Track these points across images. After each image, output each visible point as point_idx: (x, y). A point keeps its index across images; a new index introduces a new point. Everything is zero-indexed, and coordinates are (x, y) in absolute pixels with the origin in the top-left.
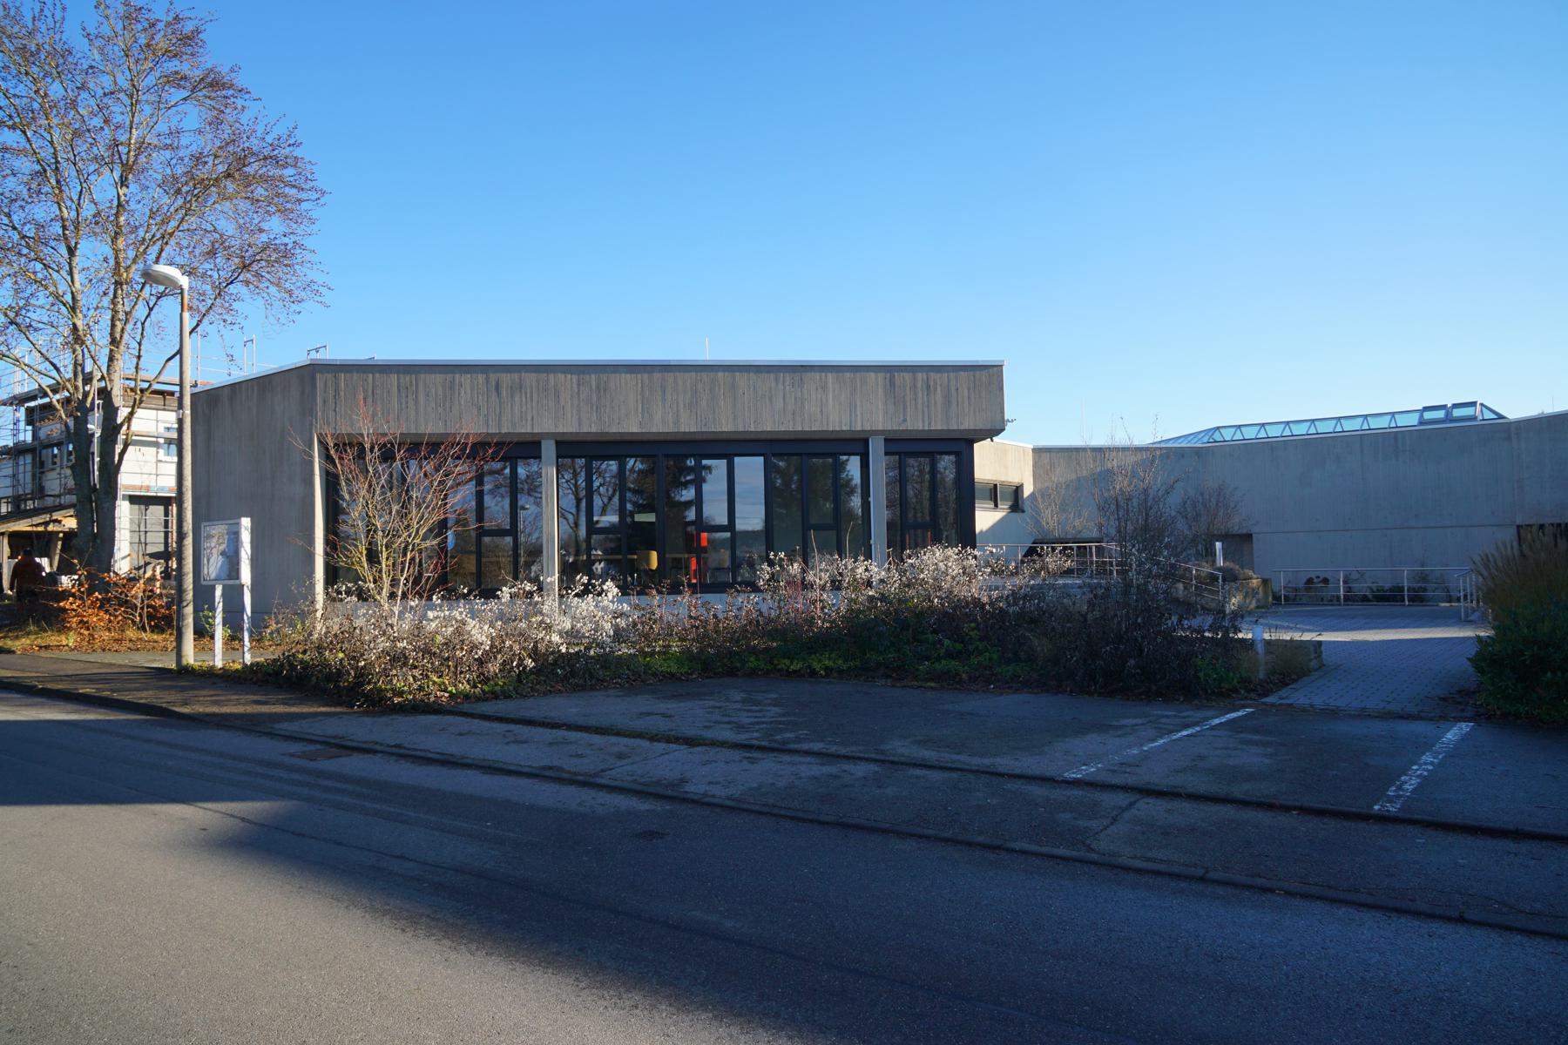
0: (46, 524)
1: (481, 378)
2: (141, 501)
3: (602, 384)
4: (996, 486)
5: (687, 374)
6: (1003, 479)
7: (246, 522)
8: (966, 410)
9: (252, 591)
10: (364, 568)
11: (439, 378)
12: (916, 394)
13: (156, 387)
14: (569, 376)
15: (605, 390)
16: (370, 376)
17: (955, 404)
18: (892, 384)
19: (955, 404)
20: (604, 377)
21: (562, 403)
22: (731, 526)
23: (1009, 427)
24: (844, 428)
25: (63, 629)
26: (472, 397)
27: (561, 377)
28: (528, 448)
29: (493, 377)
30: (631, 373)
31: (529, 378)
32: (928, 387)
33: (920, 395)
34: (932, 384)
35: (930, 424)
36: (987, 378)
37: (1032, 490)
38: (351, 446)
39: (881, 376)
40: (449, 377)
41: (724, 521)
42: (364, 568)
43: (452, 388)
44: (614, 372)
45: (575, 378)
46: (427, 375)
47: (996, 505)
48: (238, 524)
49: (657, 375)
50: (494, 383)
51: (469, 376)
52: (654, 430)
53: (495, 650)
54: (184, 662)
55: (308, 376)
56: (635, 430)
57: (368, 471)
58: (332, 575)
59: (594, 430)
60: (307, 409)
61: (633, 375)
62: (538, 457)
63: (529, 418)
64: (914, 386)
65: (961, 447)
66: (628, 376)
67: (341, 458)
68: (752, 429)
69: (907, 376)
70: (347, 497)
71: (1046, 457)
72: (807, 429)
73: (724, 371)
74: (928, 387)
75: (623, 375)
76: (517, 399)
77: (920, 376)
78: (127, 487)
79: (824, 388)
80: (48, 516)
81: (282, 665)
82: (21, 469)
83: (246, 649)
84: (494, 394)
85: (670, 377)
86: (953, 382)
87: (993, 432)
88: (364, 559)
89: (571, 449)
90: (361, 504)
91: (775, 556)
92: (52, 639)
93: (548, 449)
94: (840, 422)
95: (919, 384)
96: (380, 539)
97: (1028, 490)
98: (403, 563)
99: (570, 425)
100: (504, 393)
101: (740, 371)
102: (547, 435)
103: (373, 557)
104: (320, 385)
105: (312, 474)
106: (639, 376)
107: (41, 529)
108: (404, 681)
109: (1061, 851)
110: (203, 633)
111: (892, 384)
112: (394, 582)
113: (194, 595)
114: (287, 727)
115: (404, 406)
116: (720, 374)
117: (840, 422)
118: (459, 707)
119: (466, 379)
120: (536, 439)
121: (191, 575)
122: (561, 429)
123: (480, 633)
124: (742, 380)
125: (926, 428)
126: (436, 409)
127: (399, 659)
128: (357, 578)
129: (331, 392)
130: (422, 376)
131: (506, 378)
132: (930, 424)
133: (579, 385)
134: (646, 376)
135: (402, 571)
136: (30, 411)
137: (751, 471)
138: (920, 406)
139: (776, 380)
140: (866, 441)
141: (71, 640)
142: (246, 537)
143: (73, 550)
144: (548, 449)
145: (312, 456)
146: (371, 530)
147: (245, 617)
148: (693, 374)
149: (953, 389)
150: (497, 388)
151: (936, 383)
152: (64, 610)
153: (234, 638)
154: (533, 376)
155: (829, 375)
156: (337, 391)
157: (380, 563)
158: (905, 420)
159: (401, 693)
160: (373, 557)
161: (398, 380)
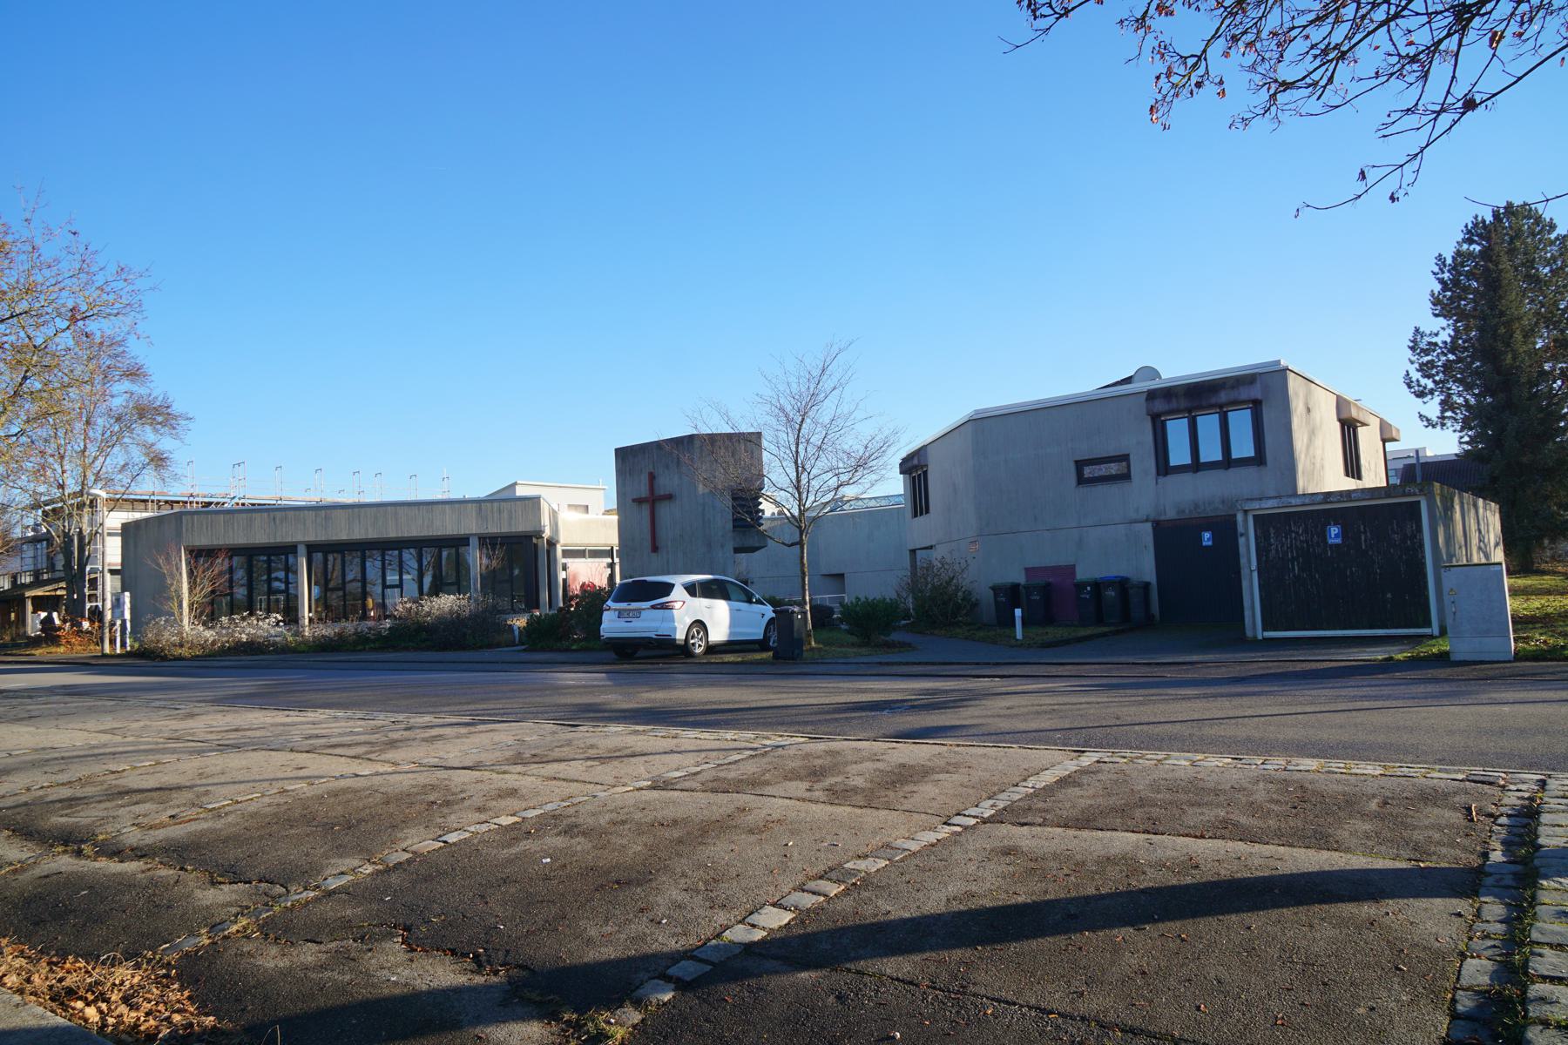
0: (56, 590)
1: (265, 515)
2: (113, 572)
13: (125, 497)
18: (480, 509)
20: (328, 512)
25: (59, 645)
28: (291, 549)
29: (272, 514)
35: (510, 525)
49: (356, 510)
53: (214, 643)
56: (345, 538)
60: (179, 534)
64: (492, 512)
69: (488, 505)
78: (109, 565)
80: (1527, 4)
82: (39, 552)
85: (363, 510)
89: (312, 548)
92: (53, 649)
93: (302, 550)
99: (311, 537)
100: (278, 522)
102: (301, 542)
107: (53, 593)
109: (1308, 709)
110: (112, 642)
111: (480, 509)
122: (307, 539)
124: (400, 510)
131: (278, 515)
136: (45, 514)
140: (468, 539)
141: (62, 649)
144: (302, 550)
152: (59, 636)
154: (292, 513)
156: (193, 524)
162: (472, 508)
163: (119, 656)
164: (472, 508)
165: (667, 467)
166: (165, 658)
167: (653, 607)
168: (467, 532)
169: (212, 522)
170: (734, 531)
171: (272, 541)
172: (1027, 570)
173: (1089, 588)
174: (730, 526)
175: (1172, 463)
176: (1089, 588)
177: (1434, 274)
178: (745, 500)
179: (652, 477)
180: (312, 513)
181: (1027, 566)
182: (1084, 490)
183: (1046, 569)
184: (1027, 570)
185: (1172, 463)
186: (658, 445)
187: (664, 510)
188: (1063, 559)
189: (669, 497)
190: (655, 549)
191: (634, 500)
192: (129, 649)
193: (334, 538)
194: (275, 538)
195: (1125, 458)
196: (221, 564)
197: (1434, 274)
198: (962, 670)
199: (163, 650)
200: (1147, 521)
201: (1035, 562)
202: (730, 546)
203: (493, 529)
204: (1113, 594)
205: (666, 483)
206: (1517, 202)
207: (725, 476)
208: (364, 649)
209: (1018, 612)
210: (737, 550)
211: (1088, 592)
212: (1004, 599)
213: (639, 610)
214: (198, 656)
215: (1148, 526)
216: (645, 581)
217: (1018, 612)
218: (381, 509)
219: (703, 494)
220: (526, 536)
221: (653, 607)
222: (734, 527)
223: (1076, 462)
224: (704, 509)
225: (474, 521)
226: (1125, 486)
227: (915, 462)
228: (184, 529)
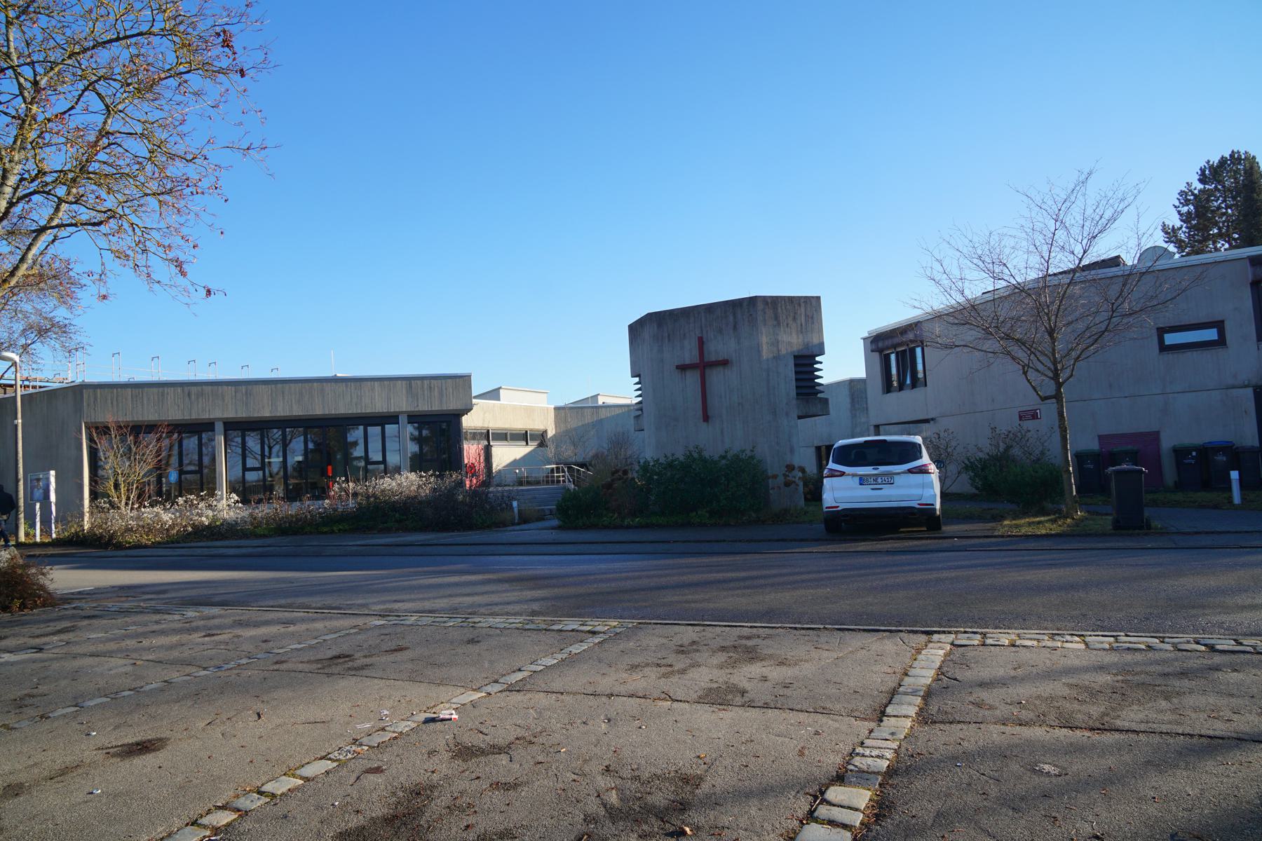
1: (179, 390)
3: (249, 391)
4: (526, 432)
5: (296, 385)
6: (532, 427)
7: (53, 473)
8: (451, 400)
9: (56, 505)
10: (112, 492)
11: (155, 390)
12: (423, 391)
14: (230, 387)
15: (250, 395)
16: (115, 390)
17: (445, 395)
18: (411, 387)
19: (445, 395)
20: (250, 387)
21: (226, 401)
22: (384, 461)
23: (475, 408)
24: (385, 411)
26: (175, 400)
27: (225, 387)
28: (209, 426)
29: (186, 389)
30: (265, 385)
31: (208, 389)
32: (430, 388)
33: (426, 392)
34: (432, 386)
35: (431, 407)
36: (462, 382)
37: (554, 432)
38: (104, 430)
39: (404, 382)
40: (161, 389)
41: (380, 459)
42: (112, 492)
43: (163, 395)
44: (256, 384)
45: (233, 388)
46: (149, 389)
47: (527, 444)
48: (49, 474)
49: (279, 386)
50: (187, 393)
51: (172, 389)
52: (278, 415)
53: (172, 527)
54: (20, 541)
55: (78, 391)
56: (267, 414)
57: (114, 448)
58: (94, 495)
59: (244, 416)
60: (78, 409)
61: (266, 386)
62: (213, 430)
63: (207, 410)
64: (423, 387)
65: (456, 416)
66: (264, 386)
67: (100, 443)
68: (333, 412)
69: (419, 382)
70: (103, 459)
71: (562, 412)
72: (363, 411)
73: (317, 382)
74: (430, 388)
75: (261, 386)
76: (200, 400)
77: (426, 382)
79: (373, 389)
81: (73, 537)
83: (53, 532)
84: (187, 399)
85: (287, 386)
86: (444, 385)
87: (822, 353)
88: (112, 488)
89: (231, 426)
90: (112, 462)
91: (340, 479)
93: (219, 427)
94: (382, 408)
95: (426, 386)
96: (121, 479)
97: (551, 433)
98: (132, 489)
99: (230, 414)
101: (326, 382)
102: (219, 419)
103: (117, 486)
104: (85, 396)
105: (81, 444)
106: (270, 386)
108: (131, 538)
112: (128, 498)
113: (24, 509)
114: (78, 555)
115: (135, 406)
116: (315, 384)
117: (382, 408)
118: (156, 545)
119: (171, 390)
120: (212, 421)
121: (22, 499)
122: (225, 416)
123: (167, 517)
124: (327, 387)
125: (430, 409)
126: (154, 406)
127: (129, 530)
128: (108, 496)
129: (92, 400)
130: (146, 389)
131: (194, 389)
132: (431, 407)
133: (235, 393)
134: (273, 386)
135: (132, 492)
137: (445, 424)
138: (426, 398)
139: (347, 386)
140: (398, 416)
142: (53, 480)
143: (806, 340)
144: (219, 427)
145: (82, 439)
146: (116, 474)
147: (53, 517)
148: (300, 384)
149: (444, 388)
150: (189, 395)
151: (434, 386)
153: (46, 522)
154: (210, 388)
155: (376, 383)
156: (95, 399)
157: (120, 489)
158: (418, 406)
159: (130, 543)
160: (117, 486)
161: (132, 391)
162: (401, 387)
163: (42, 545)
164: (401, 387)
165: (720, 331)
166: (119, 546)
167: (910, 471)
168: (398, 410)
169: (117, 396)
170: (797, 399)
171: (187, 417)
172: (1101, 437)
173: (1194, 454)
174: (793, 393)
175: (369, 428)
176: (1194, 454)
177: (1176, 207)
178: (806, 363)
179: (701, 342)
180: (231, 389)
181: (1100, 434)
182: (1169, 357)
183: (1123, 436)
184: (1101, 437)
185: (369, 428)
186: (710, 308)
187: (716, 378)
188: (1143, 426)
189: (725, 363)
190: (706, 418)
191: (678, 367)
192: (54, 536)
193: (256, 415)
194: (190, 415)
195: (1219, 325)
196: (150, 445)
197: (1176, 207)
198: (917, 546)
199: (112, 537)
200: (1246, 386)
201: (1108, 428)
202: (794, 415)
203: (424, 407)
204: (1225, 459)
205: (719, 347)
206: (1215, 160)
207: (791, 341)
208: (332, 532)
209: (1234, 475)
210: (800, 417)
211: (1193, 458)
212: (1092, 467)
213: (892, 474)
214: (159, 543)
215: (1250, 391)
216: (885, 441)
217: (1234, 475)
218: (306, 385)
219: (768, 360)
220: (454, 415)
221: (910, 471)
222: (797, 394)
223: (1222, 322)
224: (768, 375)
225: (404, 399)
226: (1220, 352)
227: (911, 336)
228: (85, 404)
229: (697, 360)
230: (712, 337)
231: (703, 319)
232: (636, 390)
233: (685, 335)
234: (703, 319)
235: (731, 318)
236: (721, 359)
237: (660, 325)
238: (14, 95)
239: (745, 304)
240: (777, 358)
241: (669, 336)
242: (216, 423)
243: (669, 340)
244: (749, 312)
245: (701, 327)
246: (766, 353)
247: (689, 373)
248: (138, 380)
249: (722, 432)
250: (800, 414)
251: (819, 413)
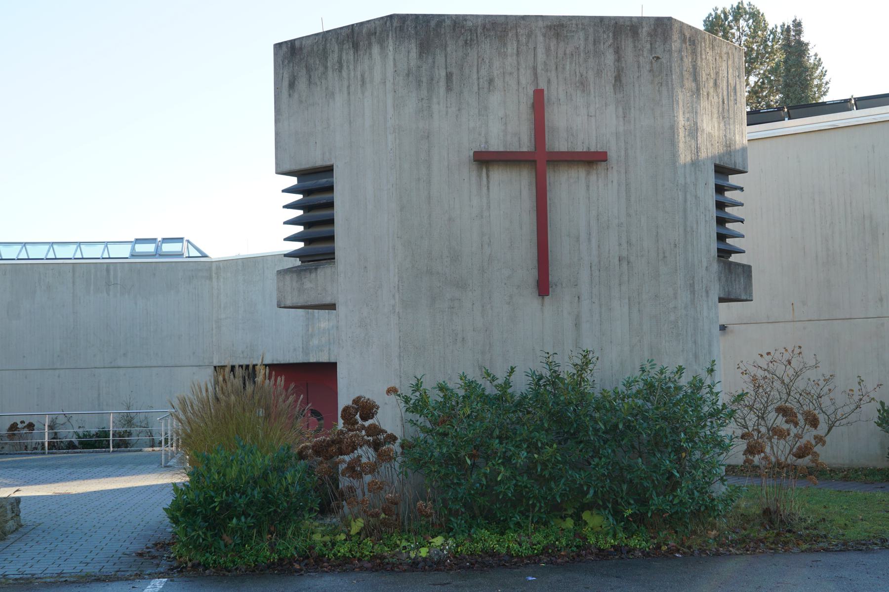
190: (543, 287)
202: (715, 296)
210: (721, 300)
229: (525, 144)
230: (562, 96)
231: (541, 51)
232: (287, 207)
233: (491, 81)
234: (541, 51)
235: (610, 58)
236: (579, 149)
237: (425, 48)
238: (104, 250)
239: (644, 31)
240: (695, 164)
241: (449, 77)
242: (181, 244)
243: (449, 89)
244: (651, 50)
245: (535, 69)
246: (684, 156)
247: (498, 175)
248: (167, 250)
249: (577, 325)
250: (722, 296)
251: (743, 297)
